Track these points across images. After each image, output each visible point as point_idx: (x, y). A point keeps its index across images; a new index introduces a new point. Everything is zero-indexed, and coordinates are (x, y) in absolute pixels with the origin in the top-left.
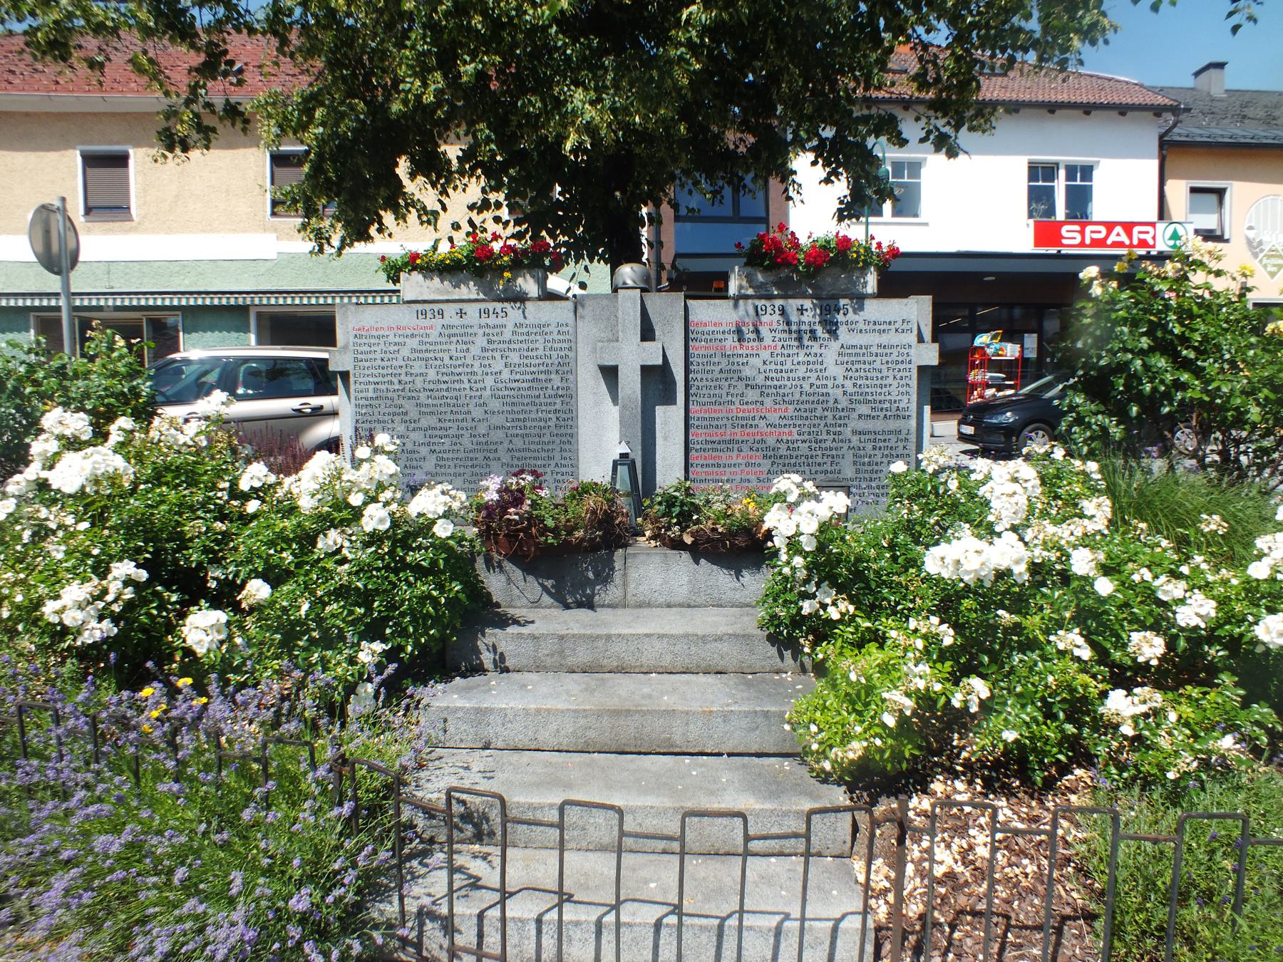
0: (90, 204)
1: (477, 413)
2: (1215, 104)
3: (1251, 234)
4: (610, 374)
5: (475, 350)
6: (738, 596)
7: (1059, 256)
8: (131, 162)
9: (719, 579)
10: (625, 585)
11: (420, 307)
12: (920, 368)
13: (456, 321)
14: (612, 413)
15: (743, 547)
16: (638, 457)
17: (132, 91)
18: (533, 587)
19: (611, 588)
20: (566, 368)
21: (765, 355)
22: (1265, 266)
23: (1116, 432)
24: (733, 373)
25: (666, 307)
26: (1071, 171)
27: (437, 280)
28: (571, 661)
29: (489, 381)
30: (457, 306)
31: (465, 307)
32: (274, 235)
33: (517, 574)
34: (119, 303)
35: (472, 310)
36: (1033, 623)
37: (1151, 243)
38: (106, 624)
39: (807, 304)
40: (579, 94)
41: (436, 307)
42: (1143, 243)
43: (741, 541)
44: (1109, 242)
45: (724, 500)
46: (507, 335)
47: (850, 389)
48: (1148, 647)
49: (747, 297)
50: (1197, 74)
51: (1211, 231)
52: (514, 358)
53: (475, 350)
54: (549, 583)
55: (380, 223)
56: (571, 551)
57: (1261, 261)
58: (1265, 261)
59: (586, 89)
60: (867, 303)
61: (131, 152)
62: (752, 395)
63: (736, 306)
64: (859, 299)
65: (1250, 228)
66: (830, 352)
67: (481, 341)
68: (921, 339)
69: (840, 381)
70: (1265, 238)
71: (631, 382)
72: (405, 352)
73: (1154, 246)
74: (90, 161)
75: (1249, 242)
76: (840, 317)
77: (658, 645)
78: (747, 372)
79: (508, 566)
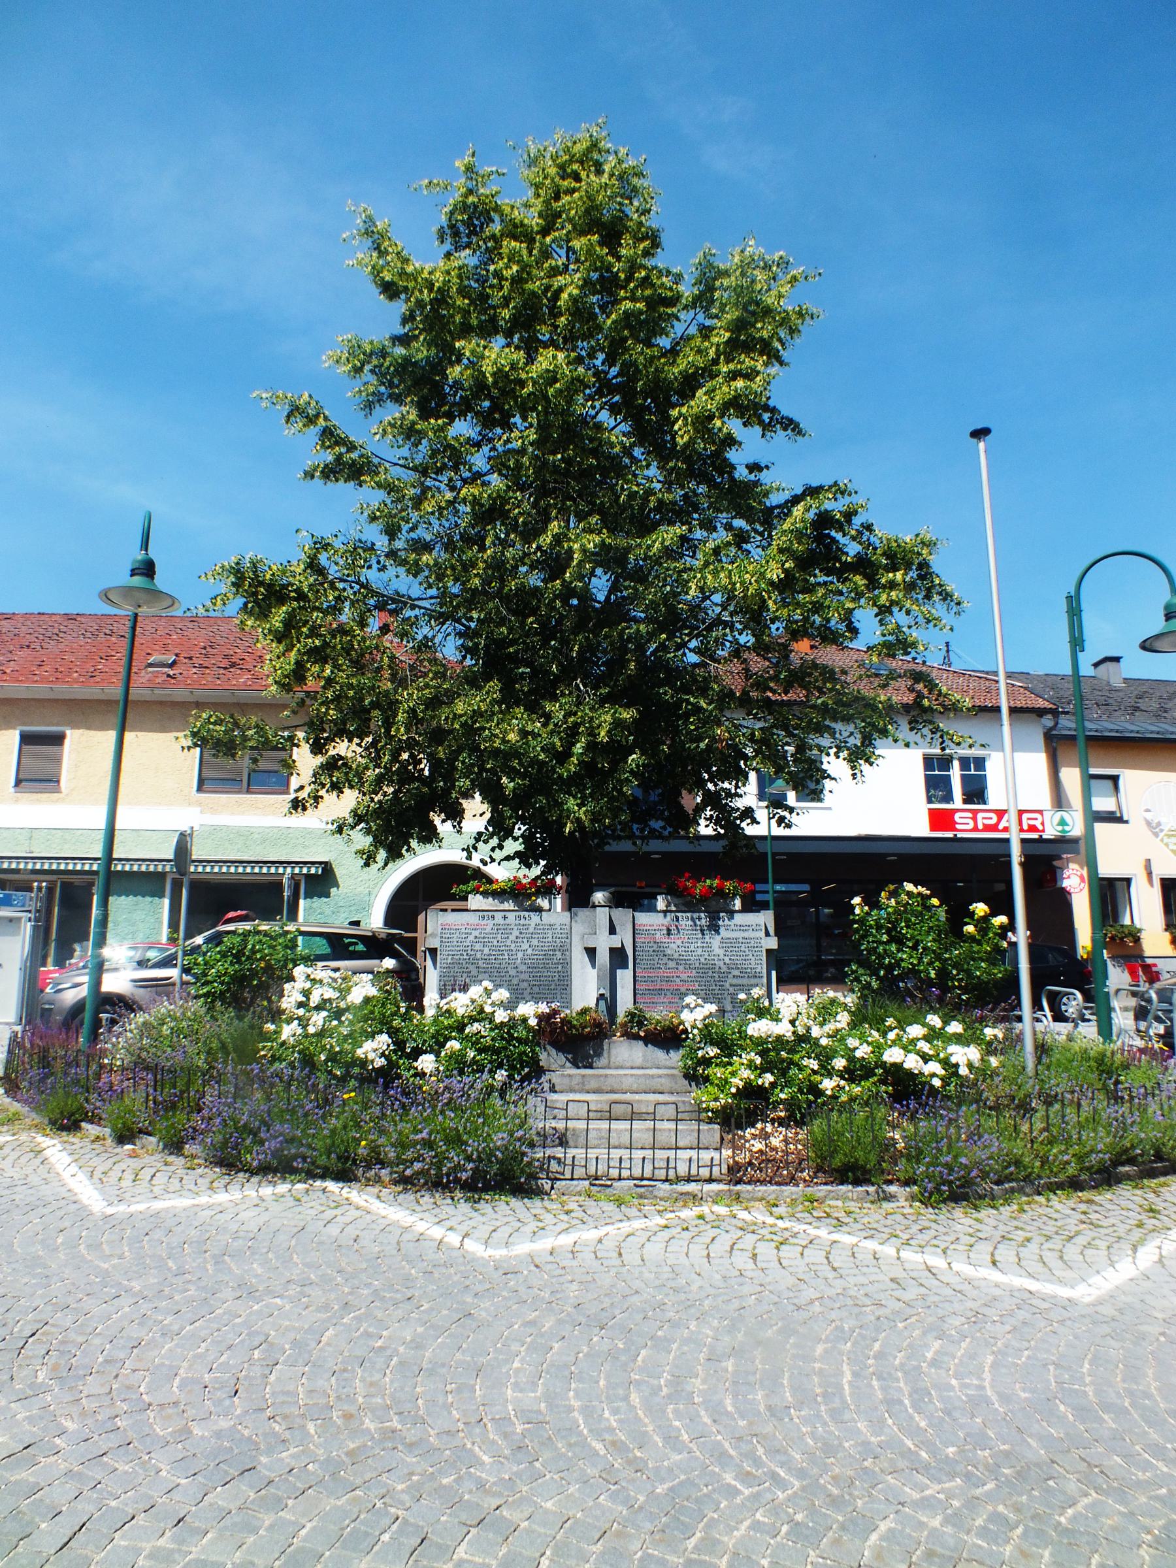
0: (21, 777)
1: (512, 972)
2: (1113, 695)
3: (1149, 816)
4: (591, 952)
5: (512, 938)
6: (668, 1063)
7: (955, 839)
8: (67, 742)
9: (659, 1054)
10: (609, 1057)
11: (481, 914)
12: (767, 951)
13: (502, 921)
14: (593, 973)
15: (669, 1037)
16: (608, 995)
17: (76, 681)
18: (562, 1058)
19: (602, 1059)
20: (565, 948)
21: (679, 942)
22: (1167, 845)
23: (875, 985)
24: (660, 952)
25: (623, 916)
26: (965, 762)
27: (490, 899)
28: (587, 1087)
29: (520, 955)
30: (503, 914)
31: (507, 914)
32: (198, 809)
33: (554, 1052)
34: (38, 867)
35: (511, 916)
36: (796, 1057)
37: (1041, 828)
38: (383, 1059)
39: (702, 915)
40: (572, 801)
41: (491, 914)
42: (1033, 829)
43: (668, 1034)
44: (1001, 827)
45: (658, 1014)
46: (531, 930)
47: (727, 961)
48: (840, 1063)
49: (671, 911)
50: (1096, 665)
51: (1113, 813)
52: (535, 942)
53: (512, 938)
54: (570, 1056)
55: (409, 847)
56: (580, 1040)
57: (1162, 840)
58: (1166, 840)
59: (575, 797)
60: (736, 916)
61: (68, 732)
62: (672, 964)
63: (665, 916)
64: (731, 913)
65: (1148, 810)
66: (715, 941)
67: (516, 933)
68: (767, 934)
69: (722, 957)
70: (1163, 820)
71: (603, 957)
72: (471, 938)
73: (1043, 831)
74: (27, 739)
75: (1148, 823)
76: (721, 923)
77: (631, 1080)
78: (668, 952)
79: (548, 1047)
